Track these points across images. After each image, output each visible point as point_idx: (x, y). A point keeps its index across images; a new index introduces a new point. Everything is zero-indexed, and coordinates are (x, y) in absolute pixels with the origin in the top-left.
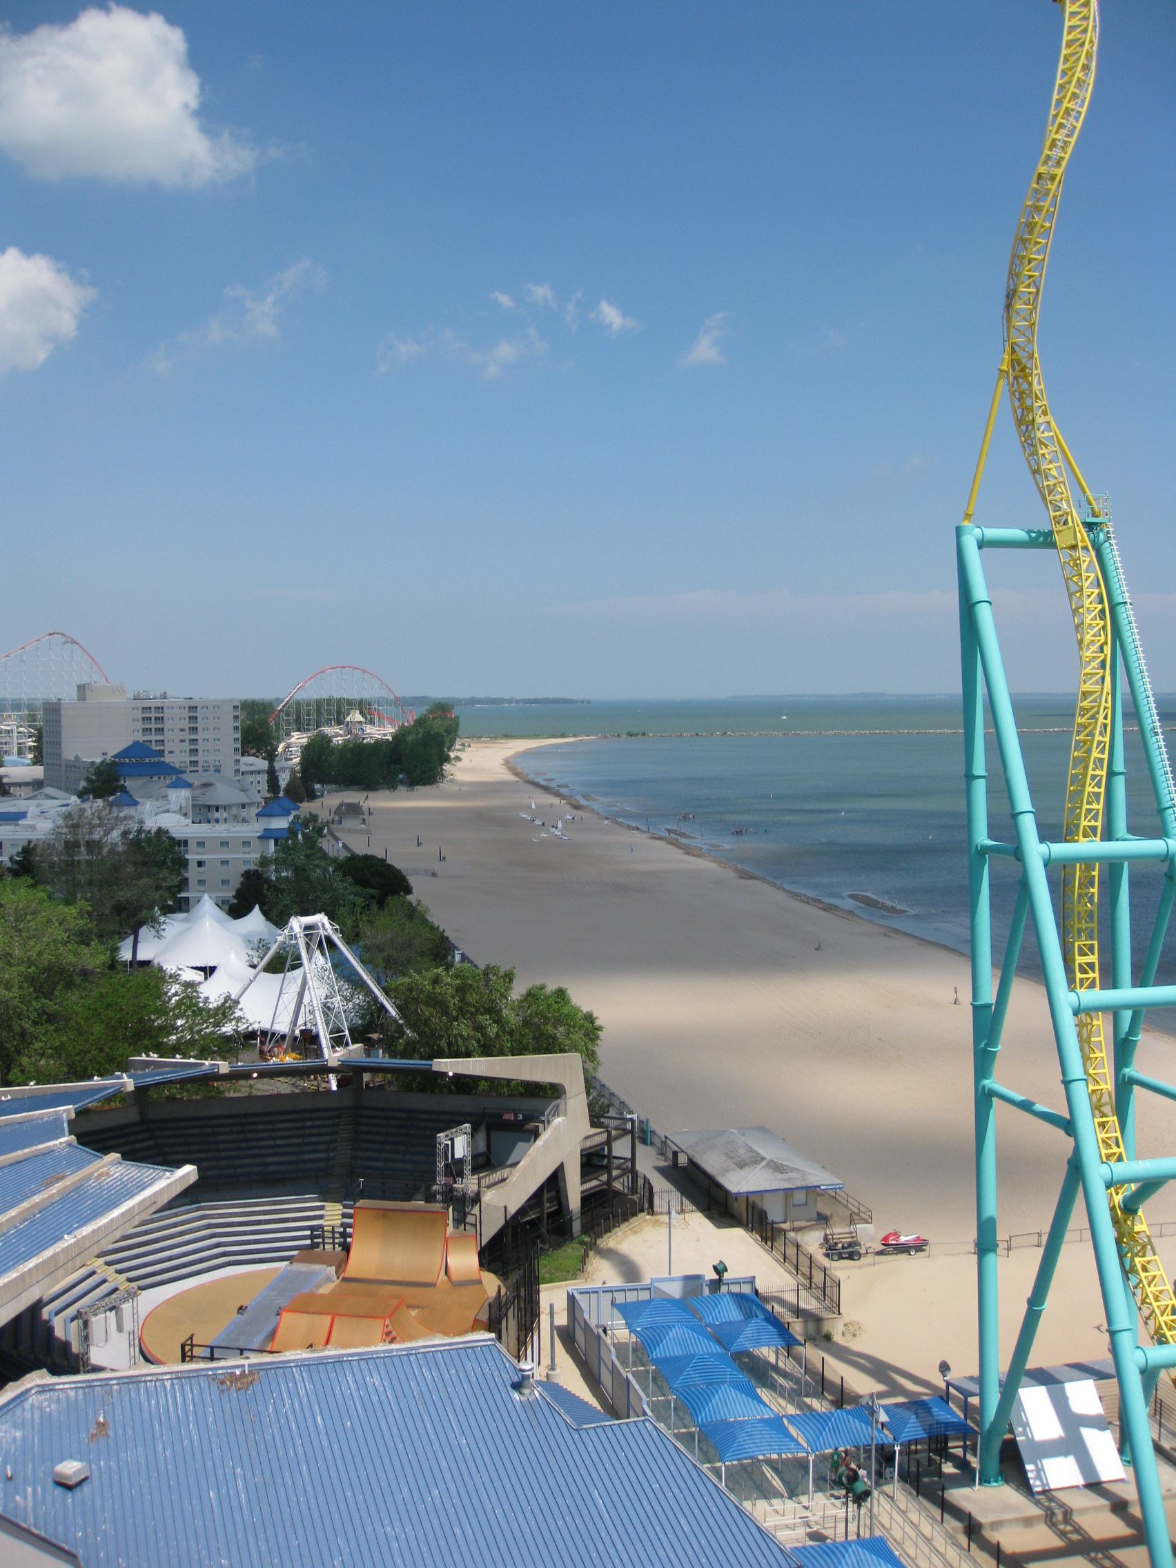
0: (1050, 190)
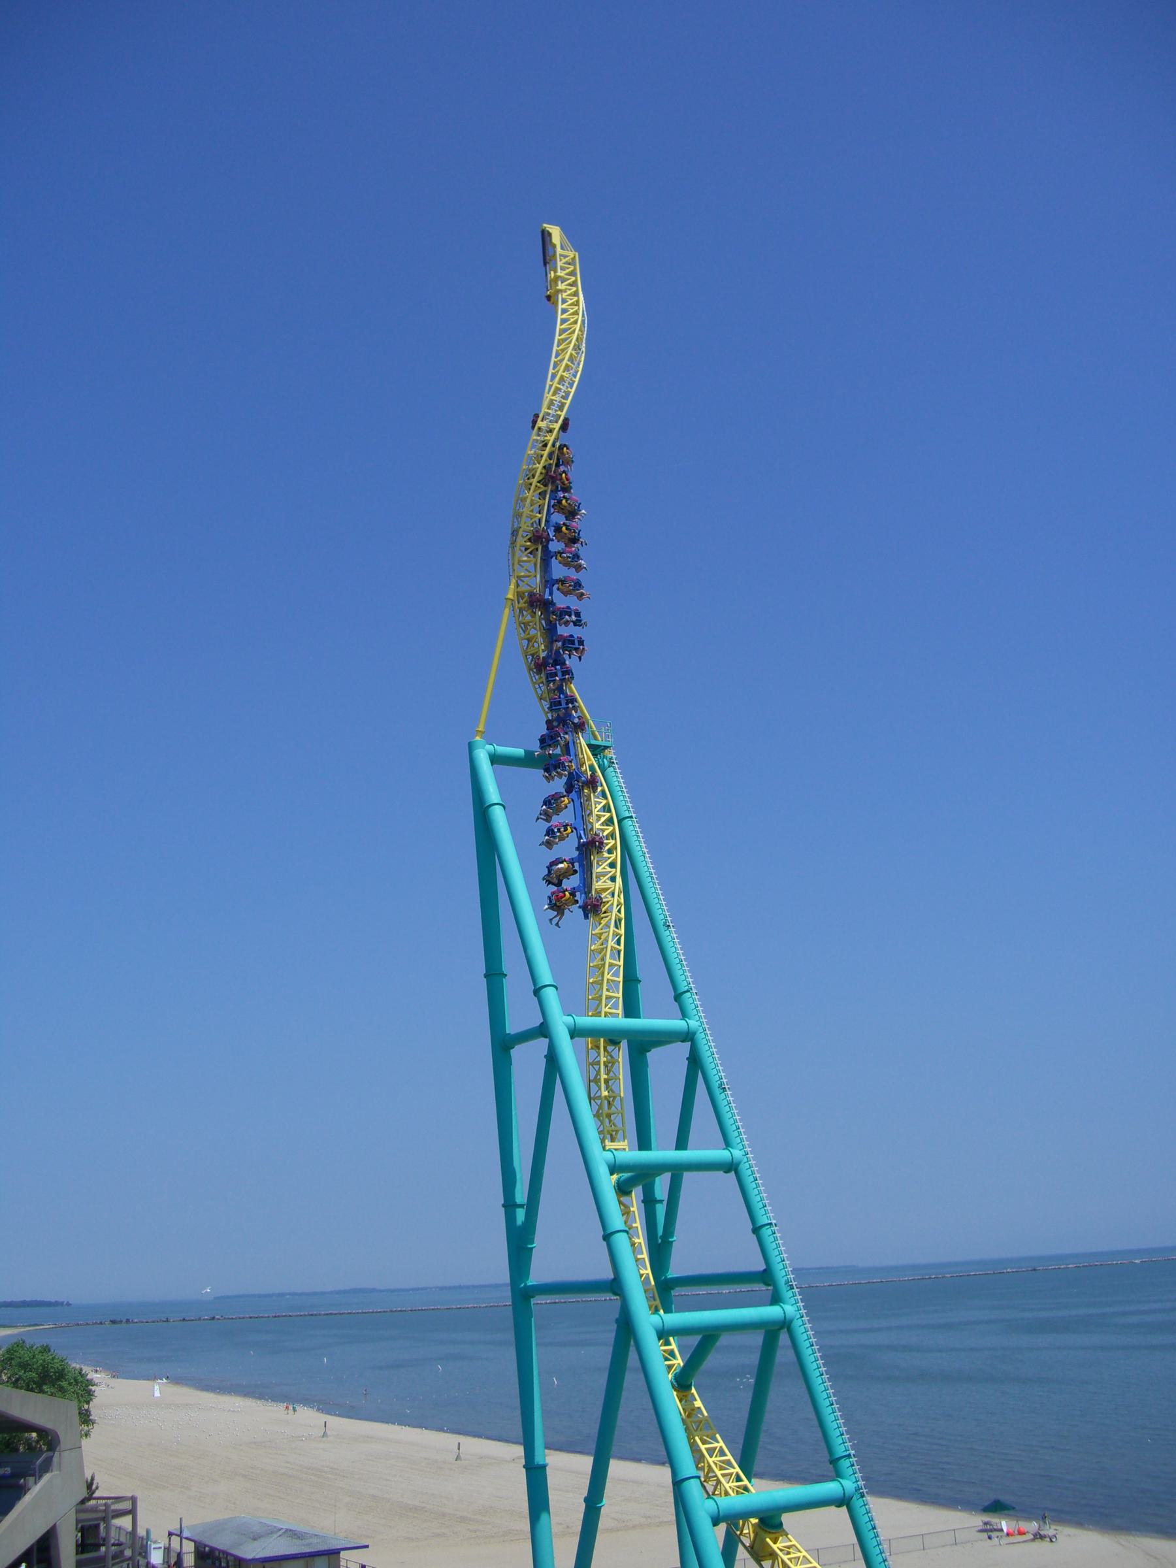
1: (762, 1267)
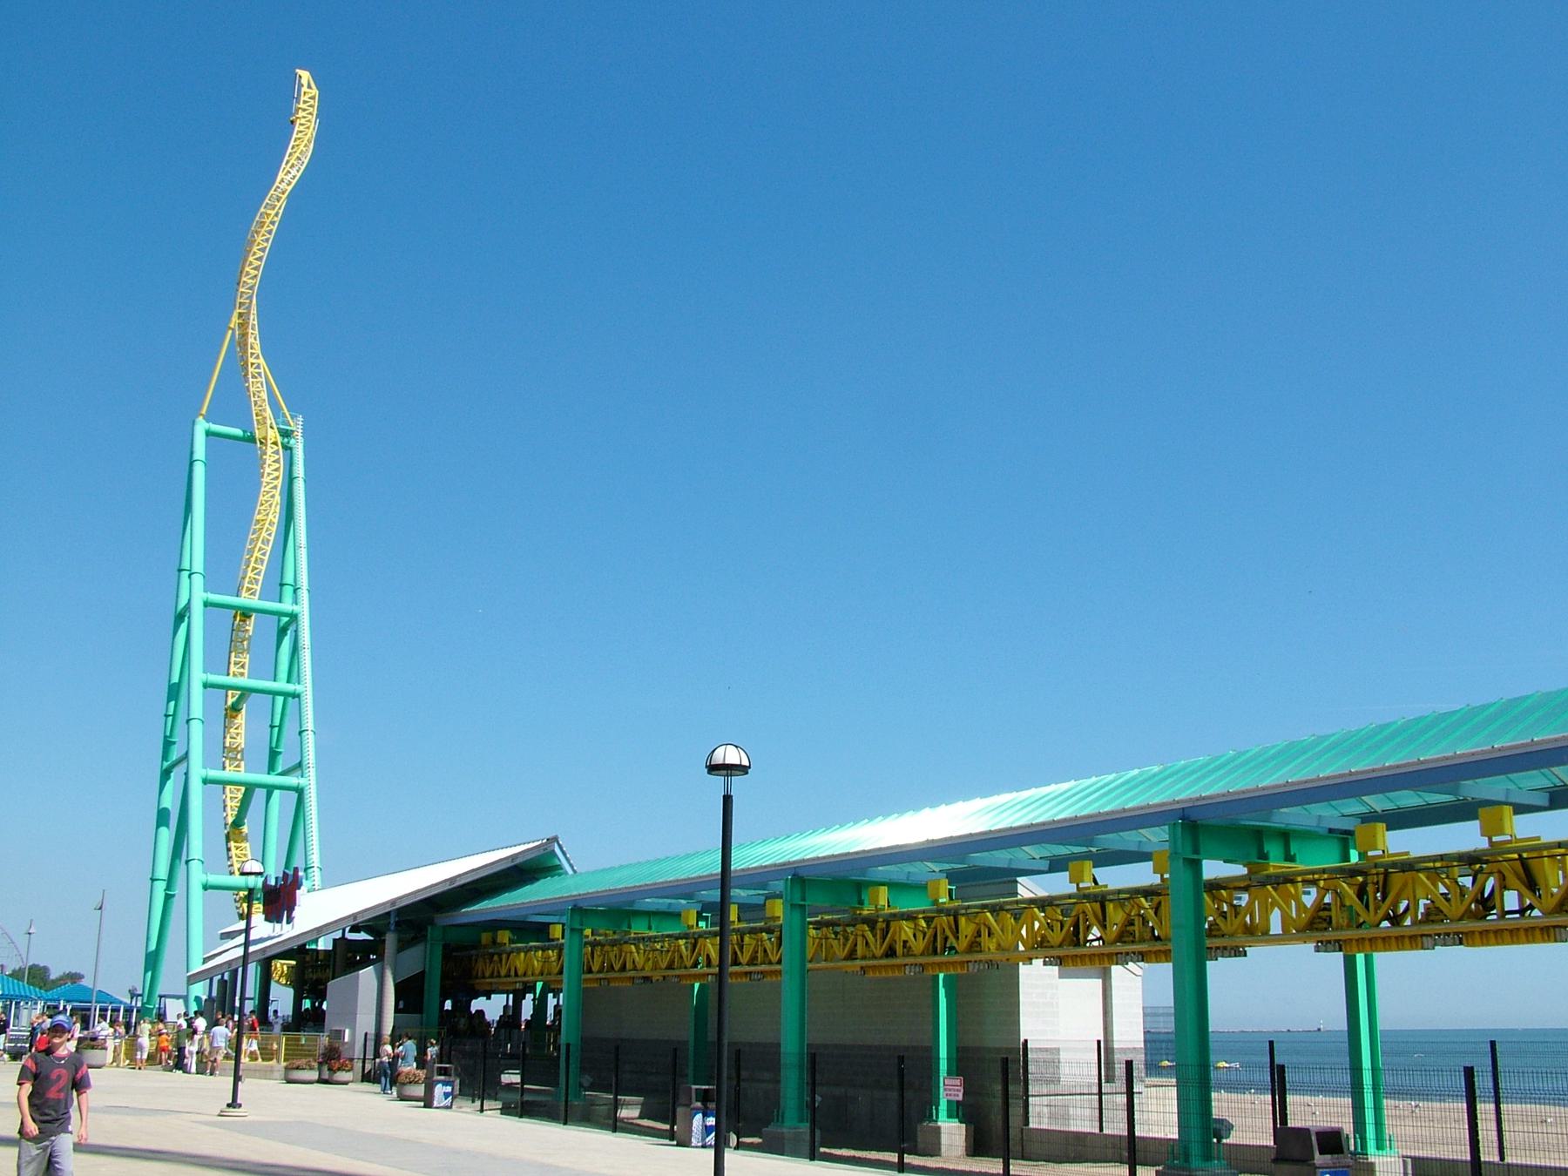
0: (276, 206)
1: (185, 994)
